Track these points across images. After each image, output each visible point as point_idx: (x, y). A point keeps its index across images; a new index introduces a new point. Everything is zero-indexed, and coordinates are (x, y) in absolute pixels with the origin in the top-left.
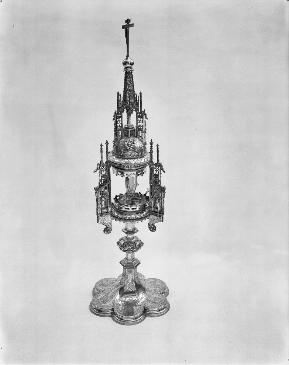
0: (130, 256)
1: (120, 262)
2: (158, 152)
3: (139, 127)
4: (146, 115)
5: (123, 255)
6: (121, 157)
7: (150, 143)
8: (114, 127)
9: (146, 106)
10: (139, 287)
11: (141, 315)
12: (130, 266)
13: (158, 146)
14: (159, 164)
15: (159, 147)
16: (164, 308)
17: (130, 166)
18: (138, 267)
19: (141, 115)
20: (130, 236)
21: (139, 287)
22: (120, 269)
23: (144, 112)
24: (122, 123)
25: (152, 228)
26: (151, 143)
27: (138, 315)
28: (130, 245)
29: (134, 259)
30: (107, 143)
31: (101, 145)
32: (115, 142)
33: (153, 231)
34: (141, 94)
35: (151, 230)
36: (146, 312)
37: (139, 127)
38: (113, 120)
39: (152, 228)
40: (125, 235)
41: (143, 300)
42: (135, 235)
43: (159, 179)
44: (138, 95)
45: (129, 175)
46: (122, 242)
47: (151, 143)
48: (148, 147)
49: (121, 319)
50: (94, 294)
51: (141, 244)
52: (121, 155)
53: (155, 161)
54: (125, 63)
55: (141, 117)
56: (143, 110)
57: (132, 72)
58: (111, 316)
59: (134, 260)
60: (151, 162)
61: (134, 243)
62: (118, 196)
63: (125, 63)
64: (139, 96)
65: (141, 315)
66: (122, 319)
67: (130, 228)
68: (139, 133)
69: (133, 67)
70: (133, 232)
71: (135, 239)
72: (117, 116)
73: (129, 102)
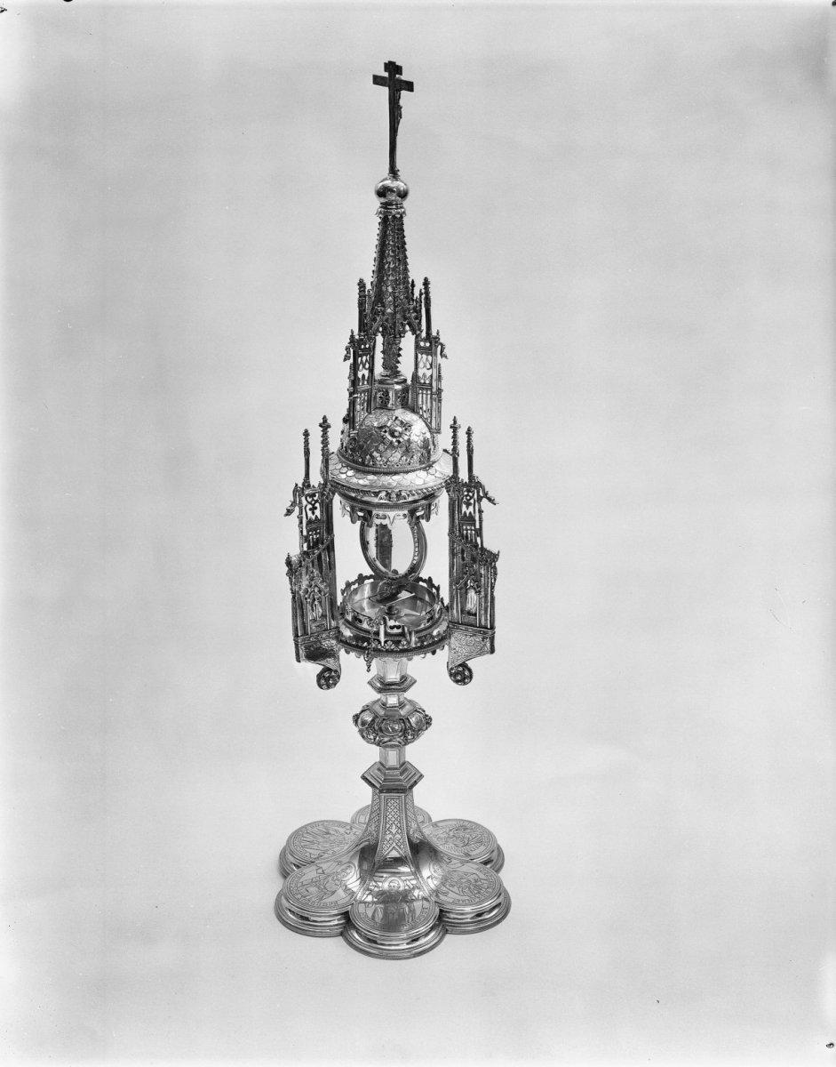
0: (392, 758)
1: (364, 778)
2: (307, 453)
3: (422, 381)
4: (442, 345)
5: (370, 754)
6: (362, 468)
7: (320, 426)
8: (347, 384)
9: (441, 322)
10: (421, 851)
11: (432, 929)
12: (393, 785)
13: (469, 433)
14: (474, 484)
15: (474, 437)
16: (494, 908)
17: (394, 496)
18: (415, 789)
19: (431, 345)
20: (392, 700)
21: (421, 851)
22: (366, 795)
23: (437, 338)
24: (371, 370)
25: (461, 674)
26: (454, 428)
27: (422, 929)
28: (391, 724)
29: (404, 766)
30: (325, 426)
31: (306, 434)
32: (349, 419)
33: (465, 684)
34: (426, 283)
35: (457, 682)
36: (444, 922)
37: (422, 381)
38: (345, 360)
39: (461, 674)
40: (376, 696)
41: (433, 884)
42: (409, 695)
43: (478, 526)
44: (419, 287)
45: (392, 519)
46: (368, 718)
47: (454, 428)
48: (444, 440)
49: (302, 918)
50: (285, 874)
51: (427, 721)
52: (356, 462)
53: (464, 476)
54: (382, 193)
55: (429, 351)
56: (434, 334)
57: (402, 217)
58: (341, 934)
59: (406, 770)
60: (452, 483)
61: (404, 720)
62: (354, 583)
63: (382, 193)
64: (423, 291)
65: (432, 929)
66: (307, 919)
67: (393, 676)
68: (421, 395)
69: (406, 203)
70: (404, 684)
71: (408, 707)
72: (359, 348)
73: (393, 305)
